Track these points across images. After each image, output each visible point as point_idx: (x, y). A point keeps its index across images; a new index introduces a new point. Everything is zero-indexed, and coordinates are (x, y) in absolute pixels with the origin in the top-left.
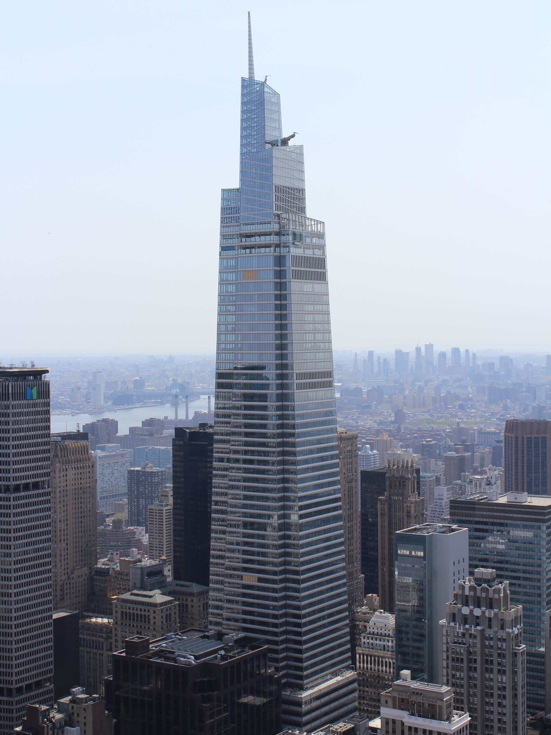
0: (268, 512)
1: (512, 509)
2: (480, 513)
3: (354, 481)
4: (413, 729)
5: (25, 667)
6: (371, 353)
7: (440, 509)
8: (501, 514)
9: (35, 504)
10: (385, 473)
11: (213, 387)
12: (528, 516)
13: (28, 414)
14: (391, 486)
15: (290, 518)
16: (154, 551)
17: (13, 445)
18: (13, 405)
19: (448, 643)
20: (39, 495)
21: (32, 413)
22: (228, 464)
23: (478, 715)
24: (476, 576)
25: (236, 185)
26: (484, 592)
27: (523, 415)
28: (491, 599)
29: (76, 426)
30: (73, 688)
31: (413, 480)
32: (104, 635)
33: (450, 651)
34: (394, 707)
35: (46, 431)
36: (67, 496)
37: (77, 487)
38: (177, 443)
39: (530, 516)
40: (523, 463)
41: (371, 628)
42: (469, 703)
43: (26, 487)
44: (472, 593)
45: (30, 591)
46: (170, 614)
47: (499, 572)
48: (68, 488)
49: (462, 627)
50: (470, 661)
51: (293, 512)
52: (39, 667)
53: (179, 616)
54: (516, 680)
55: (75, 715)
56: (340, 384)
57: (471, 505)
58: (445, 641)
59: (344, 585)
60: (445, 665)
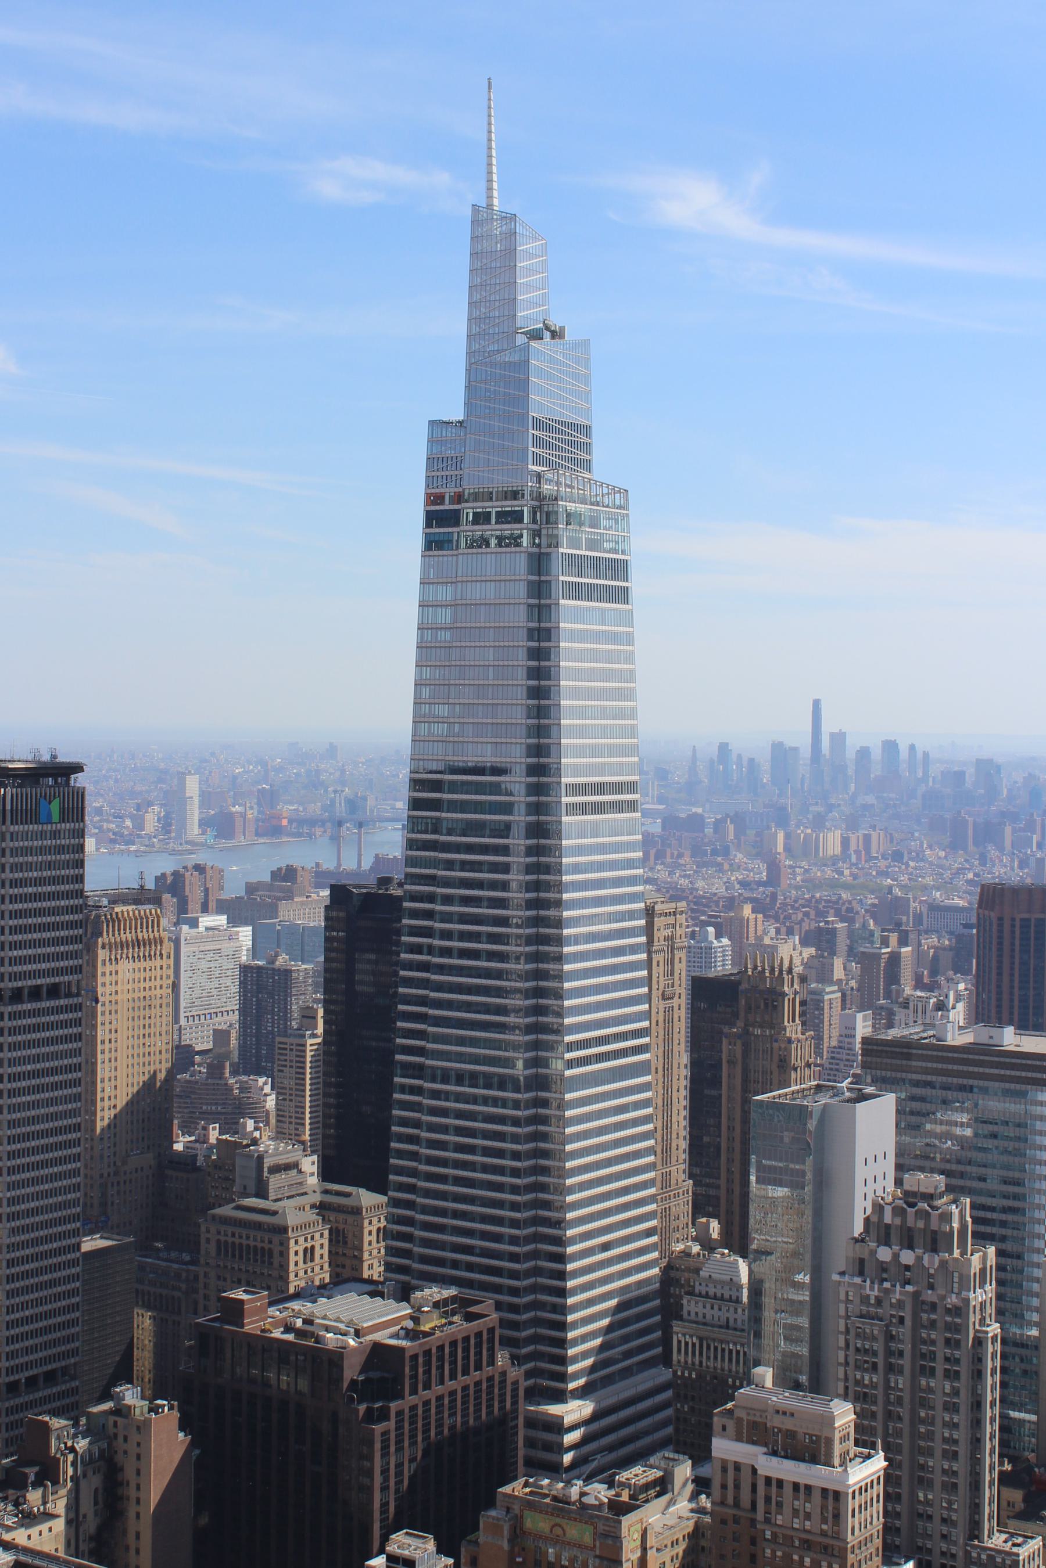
0: (506, 1054)
1: (982, 1058)
2: (919, 1064)
3: (677, 996)
4: (774, 1483)
5: (27, 1343)
6: (724, 748)
7: (848, 1054)
8: (961, 1068)
9: (50, 1026)
10: (739, 983)
11: (402, 805)
12: (1013, 1073)
13: (41, 850)
14: (750, 1008)
15: (547, 1066)
16: (286, 1126)
17: (11, 912)
18: (12, 834)
19: (848, 1317)
20: (59, 1010)
21: (49, 850)
22: (429, 958)
23: (903, 1458)
24: (906, 1187)
25: (457, 413)
26: (921, 1219)
27: (1018, 875)
28: (934, 1232)
29: (137, 876)
30: (116, 1386)
31: (792, 996)
32: (183, 1286)
33: (852, 1332)
34: (739, 1439)
35: (77, 886)
36: (116, 1012)
37: (136, 995)
38: (334, 914)
39: (1018, 1073)
40: (1012, 969)
41: (704, 1284)
42: (886, 1435)
43: (35, 993)
44: (898, 1221)
45: (38, 1196)
46: (313, 1247)
47: (955, 1182)
48: (119, 997)
49: (876, 1286)
50: (889, 1353)
51: (553, 1055)
52: (54, 1343)
53: (330, 1252)
54: (979, 1392)
55: (121, 1439)
56: (662, 807)
57: (904, 1049)
58: (842, 1312)
59: (652, 1199)
60: (842, 1360)
